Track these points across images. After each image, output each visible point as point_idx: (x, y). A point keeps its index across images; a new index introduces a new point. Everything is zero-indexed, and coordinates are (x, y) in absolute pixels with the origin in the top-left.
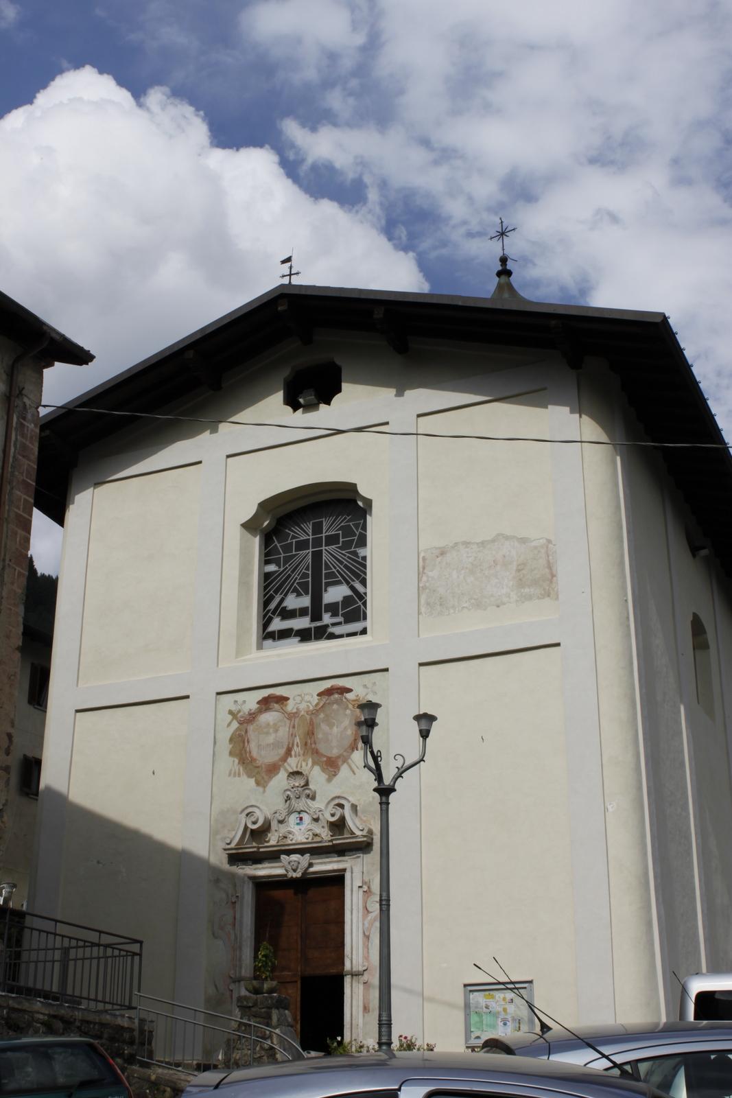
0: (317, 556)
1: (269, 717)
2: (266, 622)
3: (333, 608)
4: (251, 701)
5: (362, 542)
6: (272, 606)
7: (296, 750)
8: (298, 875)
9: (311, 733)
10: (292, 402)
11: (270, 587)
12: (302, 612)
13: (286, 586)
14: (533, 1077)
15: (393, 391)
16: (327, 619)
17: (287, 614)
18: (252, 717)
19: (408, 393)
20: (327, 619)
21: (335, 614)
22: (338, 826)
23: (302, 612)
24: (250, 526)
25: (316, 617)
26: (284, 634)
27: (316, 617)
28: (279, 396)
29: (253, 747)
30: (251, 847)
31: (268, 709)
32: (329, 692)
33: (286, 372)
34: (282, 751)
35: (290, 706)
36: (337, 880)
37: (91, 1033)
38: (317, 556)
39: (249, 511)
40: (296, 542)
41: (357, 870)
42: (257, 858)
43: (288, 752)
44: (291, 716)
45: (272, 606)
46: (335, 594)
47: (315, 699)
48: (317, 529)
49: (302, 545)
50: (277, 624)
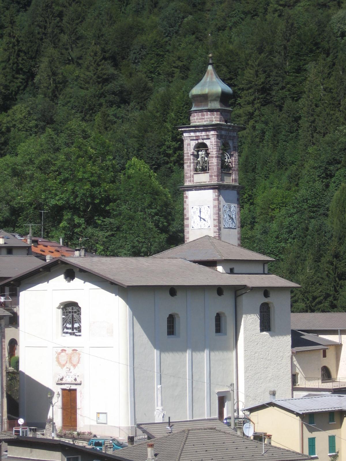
0: (73, 315)
1: (63, 354)
2: (63, 330)
3: (76, 328)
4: (59, 350)
5: (80, 315)
6: (64, 326)
7: (68, 362)
8: (68, 389)
9: (70, 359)
10: (66, 278)
11: (64, 321)
12: (70, 328)
13: (67, 322)
14: (191, 398)
15: (83, 282)
16: (75, 331)
17: (68, 328)
18: (59, 354)
19: (86, 283)
20: (75, 331)
21: (76, 330)
22: (75, 380)
23: (70, 328)
24: (59, 308)
25: (73, 330)
26: (67, 333)
27: (73, 330)
28: (62, 276)
29: (60, 360)
30: (60, 382)
31: (62, 352)
32: (74, 350)
33: (64, 271)
34: (65, 362)
35: (67, 352)
36: (75, 390)
37: (226, 79)
38: (73, 315)
39: (58, 305)
40: (19, 431)
41: (79, 389)
42: (61, 384)
43: (67, 362)
44: (67, 354)
45: (64, 326)
46: (76, 325)
47: (71, 351)
48: (73, 309)
49: (70, 312)
50: (65, 330)
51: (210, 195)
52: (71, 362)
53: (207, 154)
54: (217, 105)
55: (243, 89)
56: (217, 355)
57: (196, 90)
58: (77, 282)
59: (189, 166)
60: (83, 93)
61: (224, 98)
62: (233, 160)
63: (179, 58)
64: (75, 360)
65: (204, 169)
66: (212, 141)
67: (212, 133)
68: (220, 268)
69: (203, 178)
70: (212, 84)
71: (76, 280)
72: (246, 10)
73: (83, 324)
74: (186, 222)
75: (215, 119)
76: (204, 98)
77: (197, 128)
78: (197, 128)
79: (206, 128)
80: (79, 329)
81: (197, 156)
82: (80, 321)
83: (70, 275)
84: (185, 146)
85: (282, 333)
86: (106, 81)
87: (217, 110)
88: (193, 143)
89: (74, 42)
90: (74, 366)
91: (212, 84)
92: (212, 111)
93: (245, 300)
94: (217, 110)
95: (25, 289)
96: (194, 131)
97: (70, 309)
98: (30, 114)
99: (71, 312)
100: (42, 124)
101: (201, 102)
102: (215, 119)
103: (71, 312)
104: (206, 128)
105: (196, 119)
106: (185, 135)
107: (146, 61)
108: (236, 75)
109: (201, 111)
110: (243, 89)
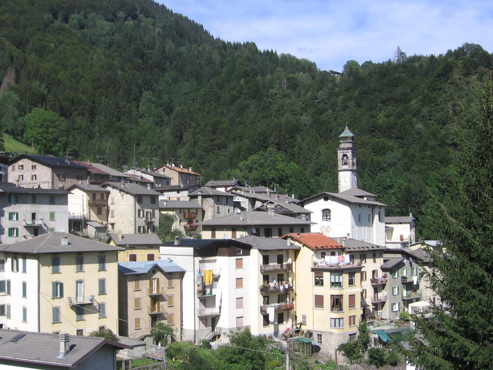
10: (324, 200)
11: (323, 216)
51: (349, 173)
52: (327, 231)
53: (347, 158)
54: (351, 141)
55: (270, 144)
56: (369, 228)
57: (342, 135)
58: (329, 201)
59: (340, 163)
60: (205, 145)
61: (353, 138)
62: (355, 160)
63: (238, 133)
64: (329, 230)
65: (345, 164)
66: (349, 154)
67: (350, 150)
68: (365, 199)
69: (346, 167)
70: (347, 133)
71: (329, 201)
72: (263, 116)
73: (332, 217)
74: (339, 183)
75: (350, 145)
76: (346, 138)
77: (343, 149)
78: (343, 149)
79: (348, 149)
80: (330, 219)
81: (343, 159)
82: (330, 216)
83: (326, 199)
84: (338, 155)
85: (383, 222)
86: (212, 141)
87: (351, 142)
88: (342, 154)
89: (197, 126)
90: (328, 232)
91: (347, 133)
92: (349, 142)
93: (377, 210)
94: (351, 142)
95: (307, 204)
96: (342, 150)
97: (326, 211)
98: (186, 152)
99: (326, 213)
100: (191, 156)
101: (345, 139)
102: (350, 145)
103: (326, 213)
104: (348, 149)
105: (342, 146)
106: (338, 151)
107: (224, 134)
108: (267, 139)
109: (345, 143)
110: (270, 144)
